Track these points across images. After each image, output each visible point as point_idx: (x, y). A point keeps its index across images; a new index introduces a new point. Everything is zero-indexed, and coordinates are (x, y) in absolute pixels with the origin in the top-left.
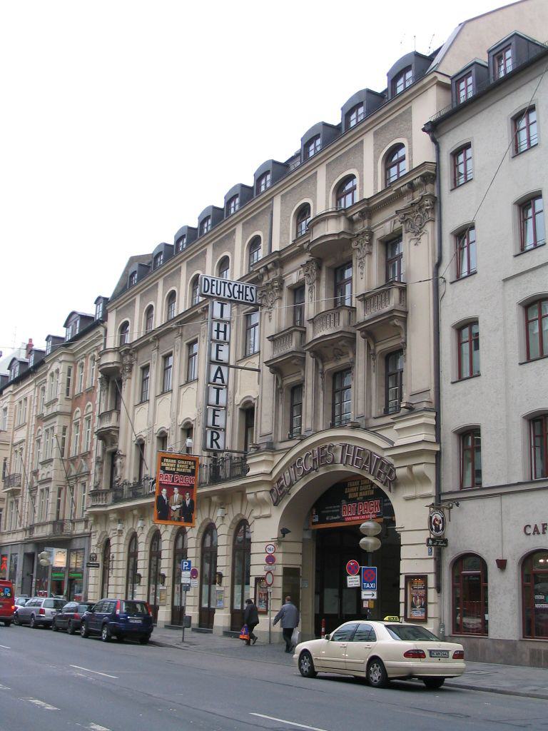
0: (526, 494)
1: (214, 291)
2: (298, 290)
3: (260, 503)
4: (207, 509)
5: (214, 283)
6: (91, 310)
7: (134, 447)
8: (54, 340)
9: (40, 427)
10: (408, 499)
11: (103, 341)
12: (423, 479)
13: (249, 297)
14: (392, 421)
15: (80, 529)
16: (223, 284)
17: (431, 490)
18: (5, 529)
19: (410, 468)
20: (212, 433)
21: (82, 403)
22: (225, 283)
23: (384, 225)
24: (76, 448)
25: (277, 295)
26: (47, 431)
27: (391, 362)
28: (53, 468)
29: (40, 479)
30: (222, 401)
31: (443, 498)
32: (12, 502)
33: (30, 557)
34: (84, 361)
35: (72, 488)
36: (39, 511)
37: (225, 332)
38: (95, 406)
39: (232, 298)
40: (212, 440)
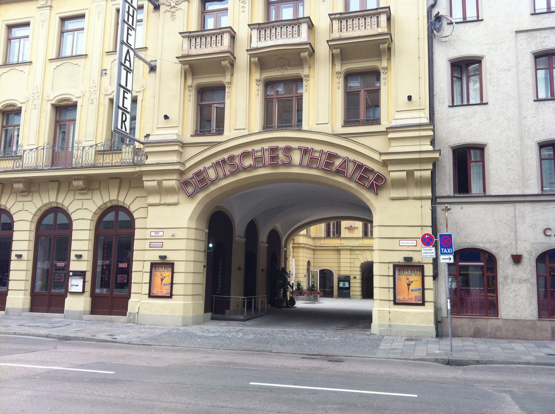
0: (546, 204)
10: (393, 199)
12: (420, 183)
31: (438, 200)
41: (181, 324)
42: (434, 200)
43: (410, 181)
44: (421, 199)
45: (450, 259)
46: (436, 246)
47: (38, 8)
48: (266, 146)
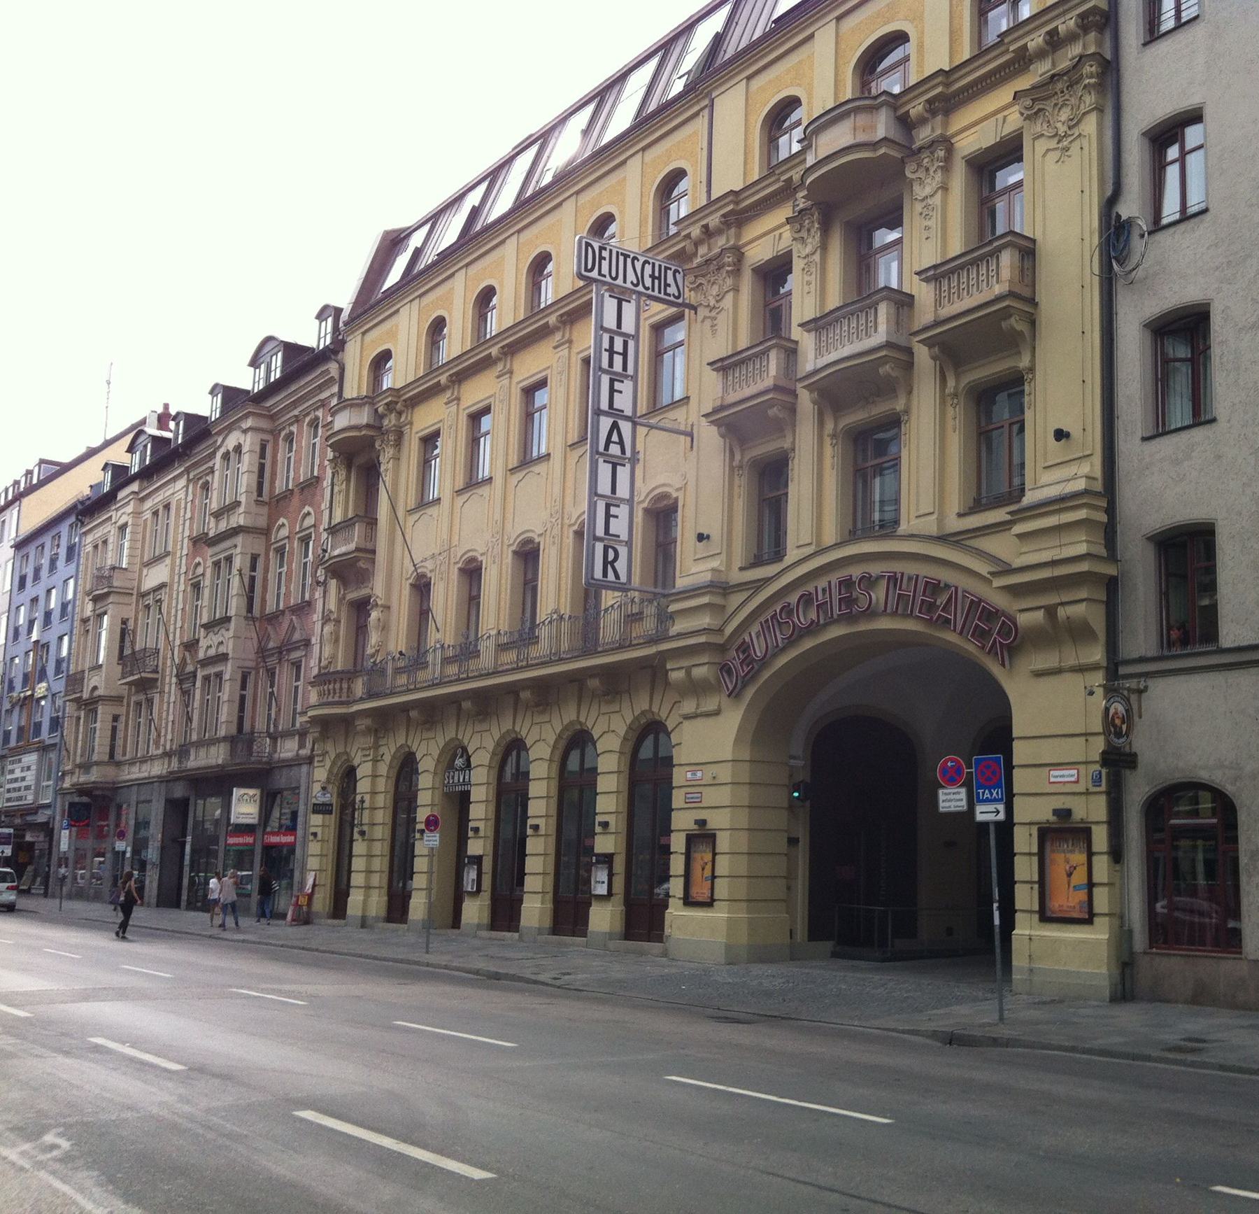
1: (605, 270)
2: (774, 274)
3: (696, 688)
4: (403, 732)
5: (605, 254)
6: (311, 335)
7: (406, 591)
8: (231, 397)
9: (198, 559)
11: (335, 389)
12: (1079, 632)
13: (672, 290)
14: (1009, 517)
15: (288, 749)
16: (621, 258)
17: (1097, 654)
18: (124, 754)
19: (688, 670)
20: (606, 549)
21: (291, 509)
22: (626, 256)
23: (977, 128)
24: (278, 595)
25: (729, 282)
26: (217, 564)
27: (995, 407)
28: (231, 633)
29: (201, 655)
30: (623, 491)
32: (139, 704)
33: (178, 810)
34: (294, 428)
35: (271, 674)
36: (200, 719)
37: (625, 354)
38: (319, 514)
39: (640, 288)
40: (606, 563)
41: (723, 961)
42: (1113, 667)
43: (1058, 632)
44: (1081, 669)
45: (998, 812)
46: (968, 785)
47: (555, 348)
48: (834, 577)
